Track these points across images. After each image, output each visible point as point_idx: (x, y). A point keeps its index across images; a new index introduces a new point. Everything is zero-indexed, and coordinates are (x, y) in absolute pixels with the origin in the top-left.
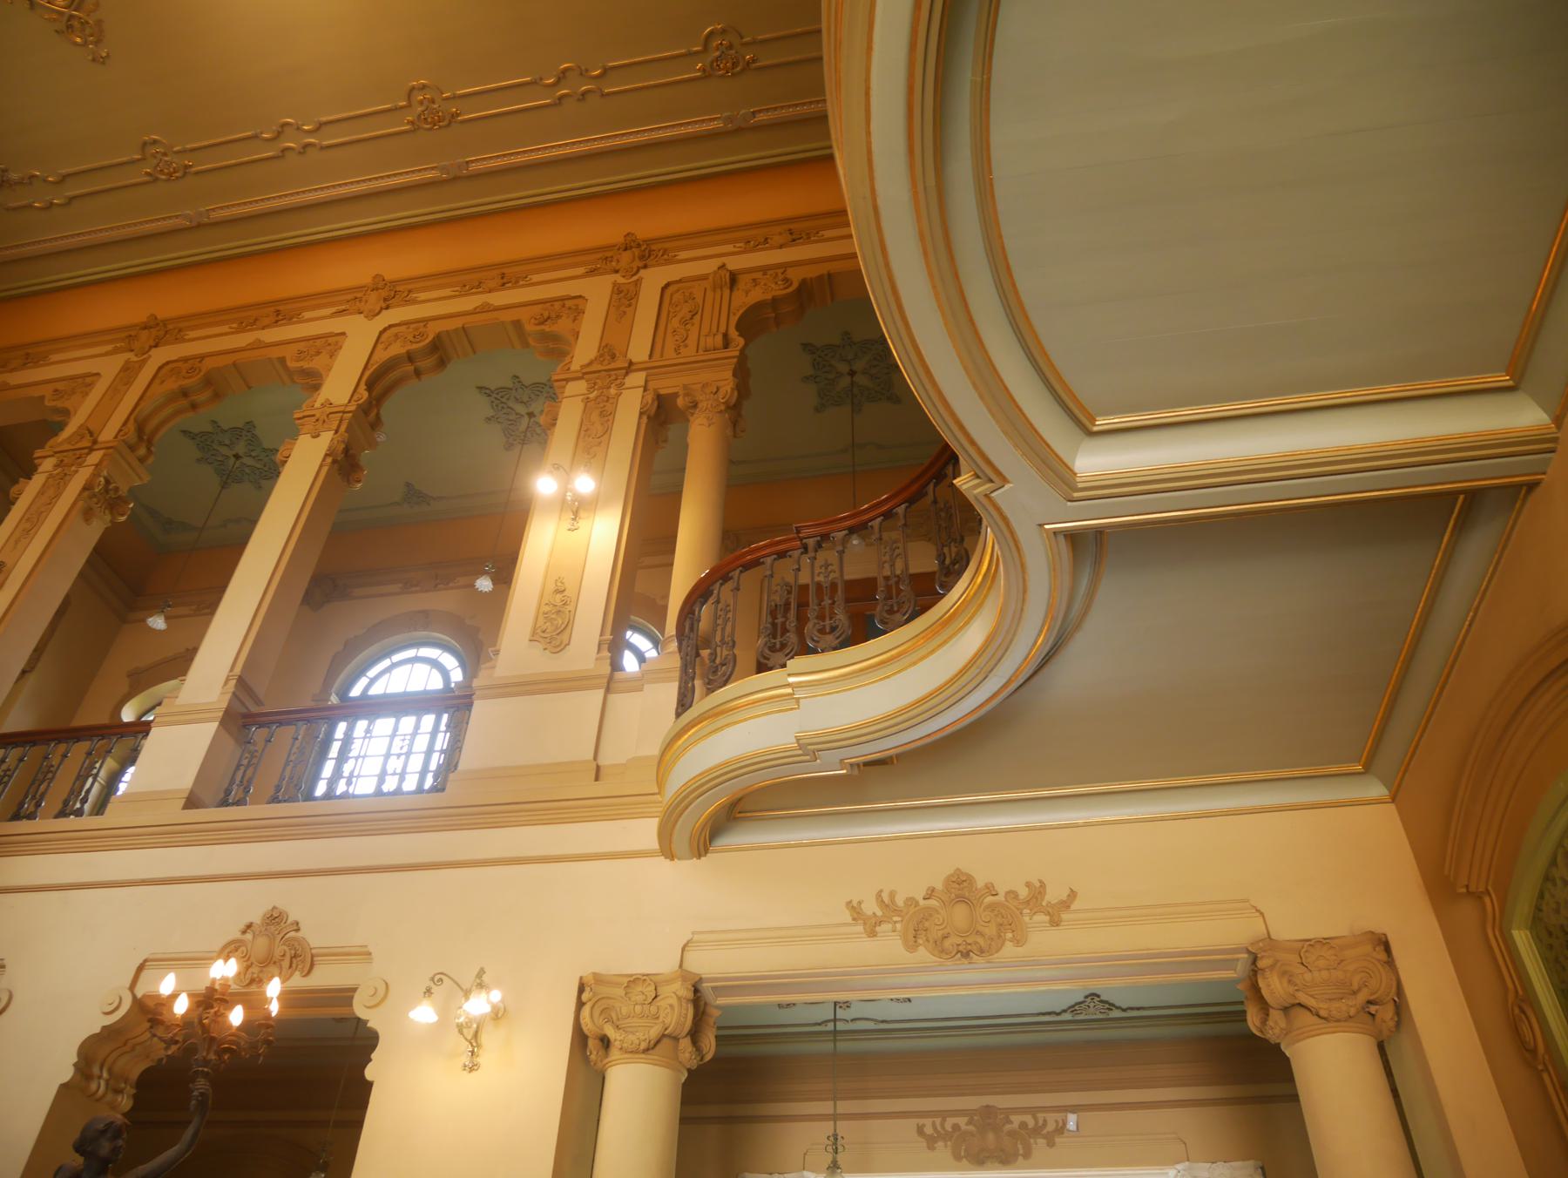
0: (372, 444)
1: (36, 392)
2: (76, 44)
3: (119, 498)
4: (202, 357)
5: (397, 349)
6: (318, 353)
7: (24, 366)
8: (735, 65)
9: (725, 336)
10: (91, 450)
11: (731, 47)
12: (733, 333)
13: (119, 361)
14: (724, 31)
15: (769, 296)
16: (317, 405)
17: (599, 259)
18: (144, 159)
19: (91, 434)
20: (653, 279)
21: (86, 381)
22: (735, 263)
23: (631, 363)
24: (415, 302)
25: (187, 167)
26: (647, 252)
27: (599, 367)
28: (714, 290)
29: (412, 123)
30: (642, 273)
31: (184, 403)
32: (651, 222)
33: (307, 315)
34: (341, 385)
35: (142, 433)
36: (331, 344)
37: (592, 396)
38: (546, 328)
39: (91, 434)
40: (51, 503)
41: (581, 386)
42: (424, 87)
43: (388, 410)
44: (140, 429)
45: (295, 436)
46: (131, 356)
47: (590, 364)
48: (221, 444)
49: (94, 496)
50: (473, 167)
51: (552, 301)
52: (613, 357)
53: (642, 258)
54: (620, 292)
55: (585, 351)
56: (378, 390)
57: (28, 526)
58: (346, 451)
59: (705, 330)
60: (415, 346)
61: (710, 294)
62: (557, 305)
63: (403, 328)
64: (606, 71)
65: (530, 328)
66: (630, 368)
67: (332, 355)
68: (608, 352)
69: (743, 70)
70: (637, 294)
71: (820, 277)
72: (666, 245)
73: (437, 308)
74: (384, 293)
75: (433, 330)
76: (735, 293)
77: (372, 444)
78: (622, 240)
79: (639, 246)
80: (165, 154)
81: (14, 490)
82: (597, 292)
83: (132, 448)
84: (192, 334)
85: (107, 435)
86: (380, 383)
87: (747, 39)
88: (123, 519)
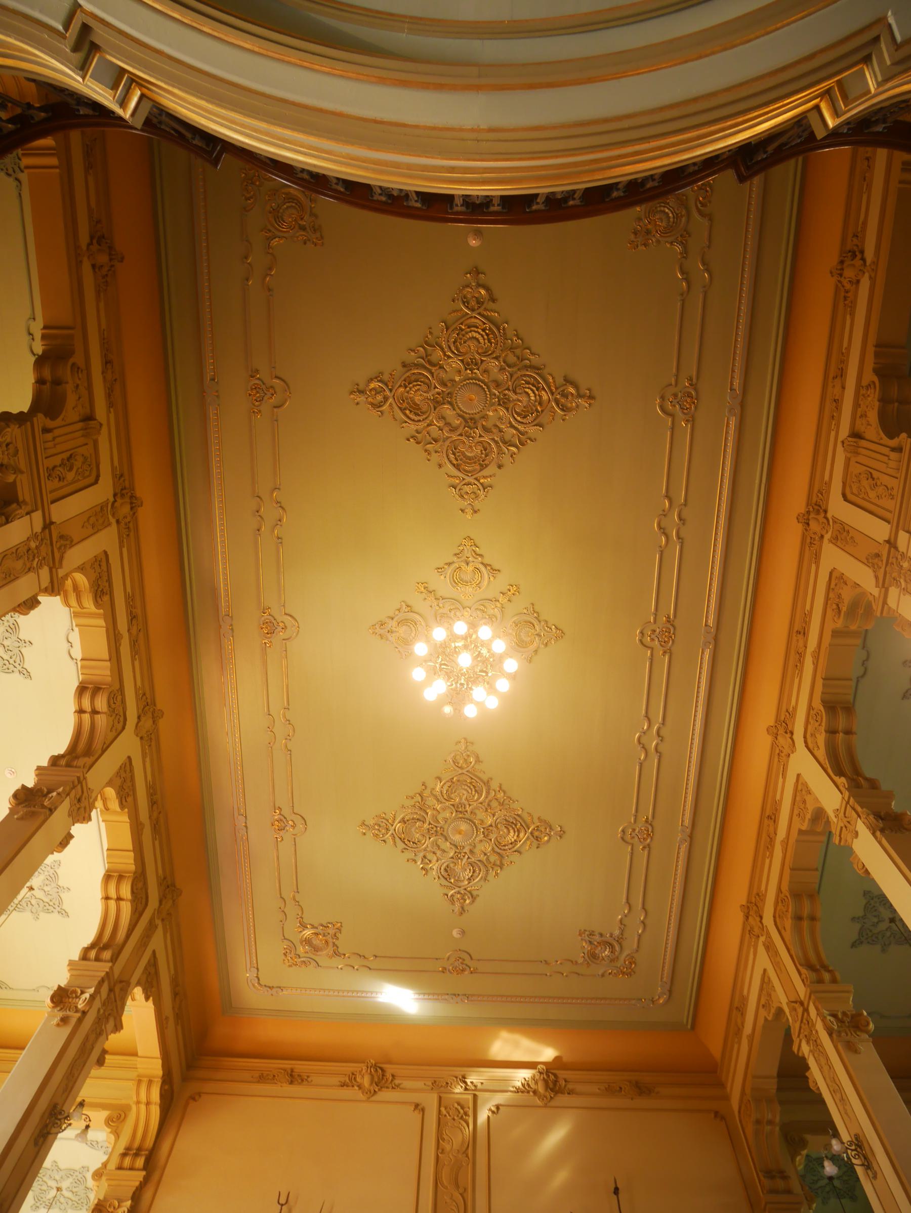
0: (890, 795)
1: (761, 1021)
2: (548, 841)
3: (853, 1016)
4: (779, 890)
5: (821, 738)
6: (804, 802)
7: (743, 1014)
8: (689, 395)
9: (893, 449)
10: (806, 1010)
11: (675, 395)
12: (894, 443)
13: (761, 949)
14: (663, 398)
15: (877, 404)
16: (835, 820)
17: (810, 548)
18: (633, 845)
19: (796, 1002)
20: (837, 508)
21: (765, 980)
22: (844, 432)
23: (888, 542)
24: (795, 709)
25: (647, 821)
26: (817, 507)
27: (882, 570)
28: (858, 454)
29: (665, 652)
30: (829, 515)
31: (806, 924)
32: (794, 498)
33: (778, 797)
34: (829, 795)
35: (815, 967)
36: (801, 788)
37: (903, 586)
38: (844, 609)
39: (796, 1002)
40: (831, 1067)
41: (893, 592)
42: (642, 633)
43: (869, 771)
44: (810, 967)
45: (850, 851)
46: (762, 939)
47: (877, 577)
48: (875, 925)
49: (839, 1032)
50: (711, 622)
51: (827, 599)
52: (878, 555)
53: (818, 513)
54: (837, 538)
55: (863, 577)
56: (847, 768)
57: (839, 1095)
58: (878, 816)
59: (882, 467)
60: (823, 724)
61: (860, 459)
62: (831, 595)
63: (810, 727)
64: (667, 496)
65: (840, 624)
66: (891, 543)
67: (809, 792)
68: (873, 560)
69: (696, 390)
70: (842, 523)
71: (877, 355)
72: (816, 491)
73: (805, 696)
74: (781, 731)
75: (818, 704)
76: (867, 436)
77: (890, 795)
78: (800, 525)
79: (808, 512)
80: (634, 830)
81: (811, 1085)
82: (832, 557)
83: (820, 981)
84: (763, 888)
85: (802, 991)
86: (842, 764)
87: (673, 383)
88: (872, 1026)
